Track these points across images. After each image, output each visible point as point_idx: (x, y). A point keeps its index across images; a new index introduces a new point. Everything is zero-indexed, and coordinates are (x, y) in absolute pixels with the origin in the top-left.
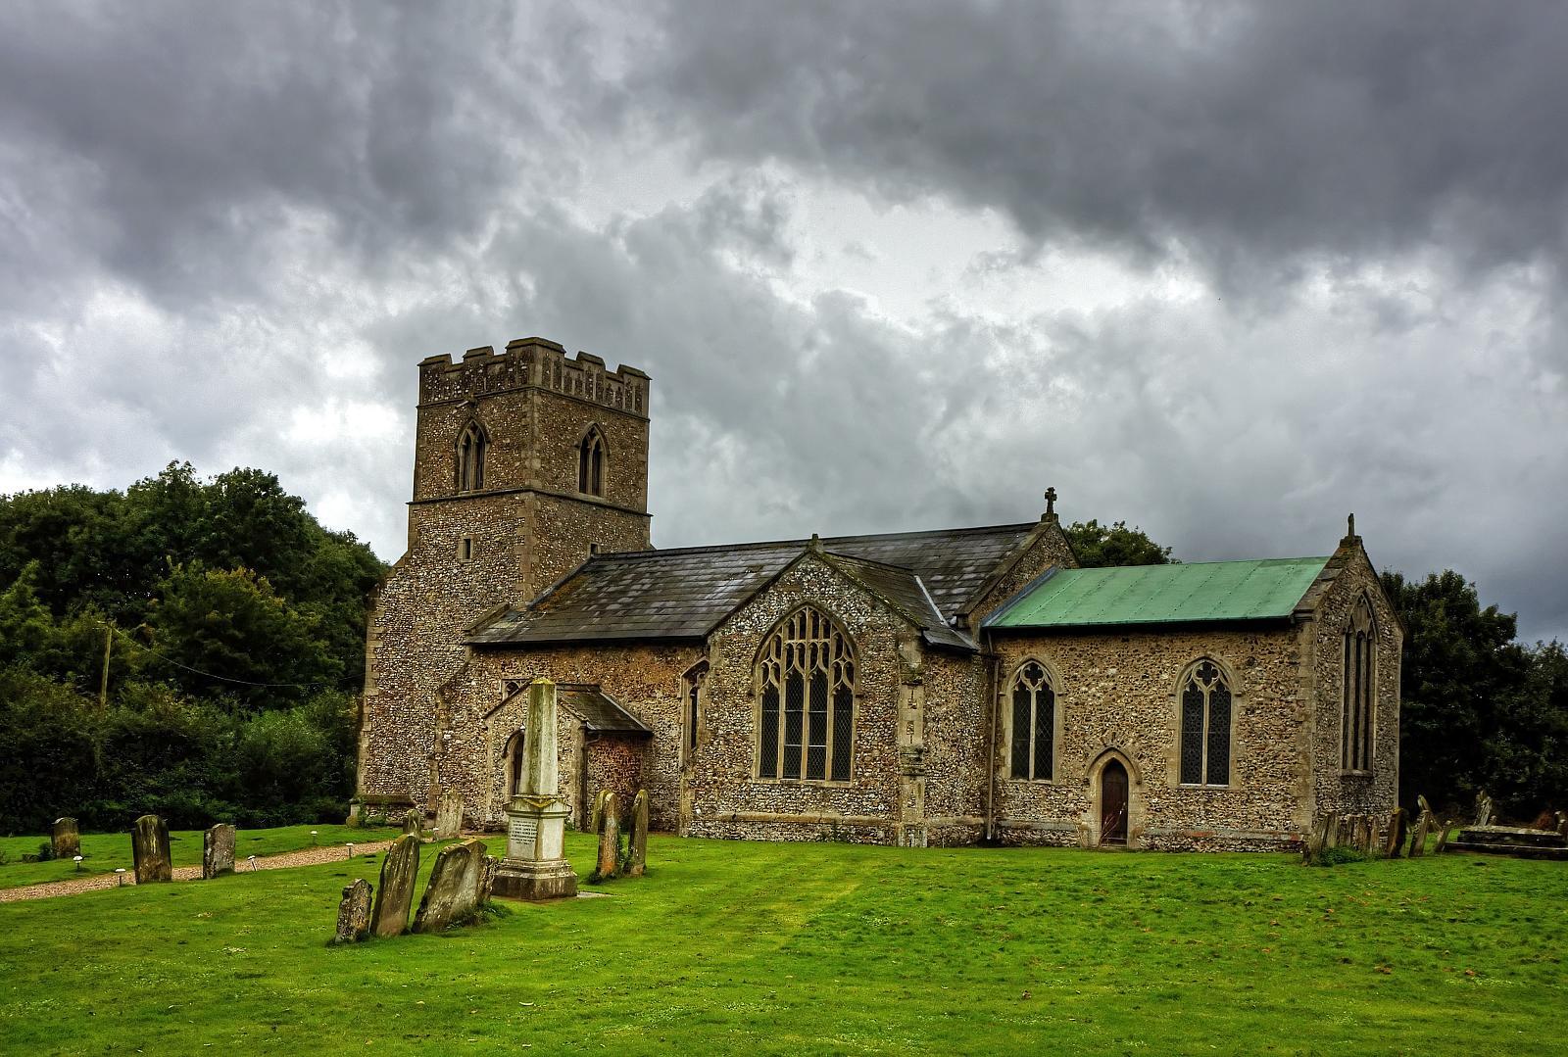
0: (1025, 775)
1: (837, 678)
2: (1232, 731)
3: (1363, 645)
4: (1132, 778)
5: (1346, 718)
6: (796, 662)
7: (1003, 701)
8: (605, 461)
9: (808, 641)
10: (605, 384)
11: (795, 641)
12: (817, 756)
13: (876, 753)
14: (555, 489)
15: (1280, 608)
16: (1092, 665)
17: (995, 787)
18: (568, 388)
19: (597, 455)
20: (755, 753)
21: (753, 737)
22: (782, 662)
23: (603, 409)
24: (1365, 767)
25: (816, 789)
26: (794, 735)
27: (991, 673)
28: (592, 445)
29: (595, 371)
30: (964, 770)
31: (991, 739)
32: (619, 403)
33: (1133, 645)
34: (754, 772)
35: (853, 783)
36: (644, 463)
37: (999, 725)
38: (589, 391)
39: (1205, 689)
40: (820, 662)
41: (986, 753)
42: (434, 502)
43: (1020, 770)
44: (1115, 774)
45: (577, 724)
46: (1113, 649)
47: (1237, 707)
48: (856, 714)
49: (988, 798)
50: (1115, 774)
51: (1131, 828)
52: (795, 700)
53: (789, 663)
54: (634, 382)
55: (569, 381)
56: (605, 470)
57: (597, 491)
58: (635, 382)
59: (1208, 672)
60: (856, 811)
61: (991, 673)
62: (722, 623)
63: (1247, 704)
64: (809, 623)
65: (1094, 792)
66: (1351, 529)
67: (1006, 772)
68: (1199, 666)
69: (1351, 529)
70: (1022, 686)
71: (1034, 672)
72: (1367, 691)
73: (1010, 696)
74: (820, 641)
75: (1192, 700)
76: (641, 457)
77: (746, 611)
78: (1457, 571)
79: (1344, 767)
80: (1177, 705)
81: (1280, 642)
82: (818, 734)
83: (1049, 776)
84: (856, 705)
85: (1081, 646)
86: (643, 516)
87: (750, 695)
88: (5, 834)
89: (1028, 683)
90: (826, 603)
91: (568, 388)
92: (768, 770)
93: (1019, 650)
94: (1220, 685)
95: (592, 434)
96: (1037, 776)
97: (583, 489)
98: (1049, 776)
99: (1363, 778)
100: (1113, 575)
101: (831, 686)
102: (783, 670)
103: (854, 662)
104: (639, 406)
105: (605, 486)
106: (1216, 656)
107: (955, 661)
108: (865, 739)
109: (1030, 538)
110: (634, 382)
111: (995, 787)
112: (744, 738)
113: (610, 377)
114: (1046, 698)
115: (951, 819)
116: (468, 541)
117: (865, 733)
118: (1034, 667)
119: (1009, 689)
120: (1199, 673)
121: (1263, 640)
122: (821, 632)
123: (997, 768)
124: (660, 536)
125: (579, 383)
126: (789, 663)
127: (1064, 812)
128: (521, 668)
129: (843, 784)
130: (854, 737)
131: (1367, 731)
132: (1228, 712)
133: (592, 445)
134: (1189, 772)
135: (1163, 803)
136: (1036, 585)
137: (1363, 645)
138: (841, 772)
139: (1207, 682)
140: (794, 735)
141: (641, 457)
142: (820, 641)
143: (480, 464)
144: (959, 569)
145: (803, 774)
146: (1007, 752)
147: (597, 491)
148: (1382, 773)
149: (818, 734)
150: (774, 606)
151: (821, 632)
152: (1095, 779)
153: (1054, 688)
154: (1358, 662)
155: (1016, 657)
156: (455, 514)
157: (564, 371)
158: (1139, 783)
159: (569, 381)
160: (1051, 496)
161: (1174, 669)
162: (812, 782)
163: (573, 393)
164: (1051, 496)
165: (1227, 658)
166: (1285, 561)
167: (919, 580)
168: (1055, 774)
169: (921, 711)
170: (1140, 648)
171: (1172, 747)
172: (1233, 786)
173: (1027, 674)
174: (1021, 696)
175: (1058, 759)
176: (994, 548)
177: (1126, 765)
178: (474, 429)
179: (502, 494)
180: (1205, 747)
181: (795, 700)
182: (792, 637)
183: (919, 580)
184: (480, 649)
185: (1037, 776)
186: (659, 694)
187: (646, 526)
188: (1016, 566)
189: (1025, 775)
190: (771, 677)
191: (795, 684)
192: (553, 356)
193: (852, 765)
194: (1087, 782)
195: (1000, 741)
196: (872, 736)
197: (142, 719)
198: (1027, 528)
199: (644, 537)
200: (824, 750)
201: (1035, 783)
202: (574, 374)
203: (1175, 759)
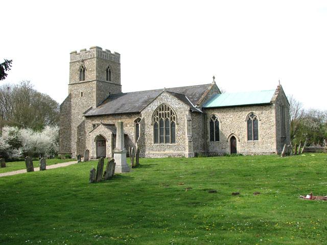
0: (213, 141)
1: (171, 120)
2: (259, 129)
4: (237, 140)
8: (111, 73)
9: (167, 112)
11: (161, 112)
13: (181, 137)
14: (102, 80)
15: (268, 101)
19: (110, 72)
25: (168, 145)
27: (205, 118)
28: (109, 70)
29: (109, 53)
31: (205, 133)
37: (207, 129)
39: (251, 119)
41: (204, 136)
42: (74, 84)
43: (212, 139)
45: (111, 133)
47: (259, 123)
48: (176, 128)
54: (117, 56)
55: (103, 55)
56: (112, 75)
57: (110, 80)
58: (117, 55)
59: (252, 115)
61: (205, 118)
65: (229, 144)
67: (209, 140)
70: (212, 120)
71: (214, 117)
74: (167, 112)
75: (249, 122)
77: (149, 106)
80: (246, 123)
81: (268, 107)
82: (167, 133)
84: (176, 125)
85: (225, 110)
86: (120, 86)
89: (251, 118)
90: (168, 103)
92: (156, 141)
95: (109, 67)
97: (107, 80)
98: (219, 140)
100: (118, 109)
104: (118, 61)
105: (112, 79)
106: (254, 112)
110: (117, 56)
116: (82, 93)
117: (178, 132)
118: (214, 116)
119: (209, 121)
122: (167, 110)
123: (207, 139)
124: (124, 91)
125: (106, 56)
127: (222, 148)
128: (96, 122)
129: (174, 144)
130: (176, 133)
131: (285, 128)
133: (109, 70)
140: (161, 133)
143: (84, 75)
146: (209, 135)
147: (110, 80)
150: (156, 104)
151: (167, 110)
153: (258, 118)
156: (79, 87)
159: (103, 55)
160: (214, 78)
161: (245, 114)
164: (214, 78)
165: (257, 113)
169: (191, 126)
171: (245, 133)
173: (213, 117)
174: (212, 122)
177: (236, 137)
178: (83, 67)
179: (90, 82)
182: (160, 111)
184: (87, 117)
186: (128, 125)
187: (121, 88)
191: (161, 121)
192: (100, 50)
195: (207, 134)
197: (238, 168)
199: (120, 91)
201: (216, 142)
202: (105, 54)
203: (246, 136)
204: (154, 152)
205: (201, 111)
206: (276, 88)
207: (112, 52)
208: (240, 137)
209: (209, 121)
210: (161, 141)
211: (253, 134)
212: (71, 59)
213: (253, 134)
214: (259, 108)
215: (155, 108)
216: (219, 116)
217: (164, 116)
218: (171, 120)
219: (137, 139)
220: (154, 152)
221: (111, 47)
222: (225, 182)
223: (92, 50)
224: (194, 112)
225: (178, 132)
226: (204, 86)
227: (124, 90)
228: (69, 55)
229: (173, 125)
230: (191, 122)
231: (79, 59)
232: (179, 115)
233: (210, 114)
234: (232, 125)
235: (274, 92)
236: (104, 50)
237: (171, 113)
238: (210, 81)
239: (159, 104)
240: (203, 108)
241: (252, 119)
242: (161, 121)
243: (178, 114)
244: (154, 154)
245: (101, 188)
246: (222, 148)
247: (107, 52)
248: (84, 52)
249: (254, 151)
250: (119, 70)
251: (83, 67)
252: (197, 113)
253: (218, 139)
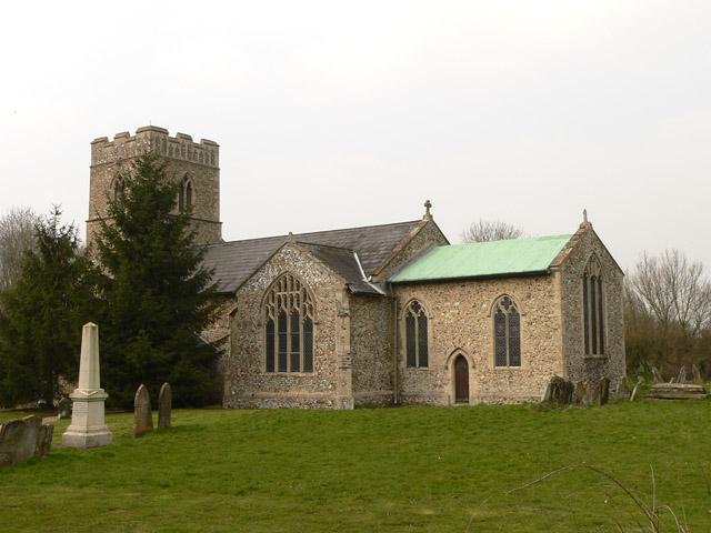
0: (414, 365)
3: (596, 284)
4: (470, 364)
5: (586, 326)
6: (283, 306)
7: (400, 323)
8: (194, 193)
9: (294, 293)
10: (193, 150)
12: (295, 360)
15: (542, 266)
16: (447, 301)
17: (398, 373)
18: (171, 153)
19: (189, 189)
20: (263, 357)
21: (261, 349)
22: (275, 305)
23: (192, 164)
24: (602, 352)
25: (295, 377)
26: (283, 347)
27: (393, 308)
29: (187, 143)
30: (379, 364)
32: (202, 161)
33: (467, 288)
34: (263, 368)
35: (315, 374)
36: (217, 193)
38: (183, 155)
39: (504, 311)
40: (295, 305)
41: (391, 354)
43: (411, 363)
44: (461, 363)
46: (457, 290)
47: (523, 321)
48: (315, 334)
49: (394, 380)
50: (461, 363)
51: (470, 395)
52: (283, 327)
53: (279, 305)
54: (210, 149)
58: (210, 148)
59: (507, 302)
60: (317, 390)
62: (244, 284)
63: (528, 320)
64: (289, 283)
65: (450, 374)
66: (586, 219)
67: (403, 364)
68: (502, 299)
69: (586, 219)
70: (410, 313)
71: (416, 306)
72: (601, 309)
73: (404, 319)
75: (499, 319)
76: (215, 190)
78: (126, 119)
79: (587, 352)
80: (491, 322)
81: (542, 284)
82: (295, 347)
83: (519, 365)
84: (315, 327)
85: (441, 290)
87: (259, 325)
88: (643, 351)
91: (171, 153)
92: (270, 368)
93: (407, 294)
94: (513, 310)
95: (186, 179)
96: (420, 366)
99: (600, 359)
101: (302, 318)
102: (276, 310)
103: (312, 303)
107: (369, 302)
108: (319, 347)
109: (416, 229)
110: (210, 149)
111: (398, 373)
112: (257, 350)
113: (196, 146)
114: (423, 320)
115: (372, 393)
117: (319, 344)
118: (416, 303)
119: (403, 316)
120: (502, 304)
121: (534, 283)
123: (399, 361)
124: (228, 235)
126: (279, 305)
127: (435, 386)
130: (314, 347)
132: (519, 325)
133: (186, 185)
134: (500, 361)
135: (487, 378)
136: (420, 255)
137: (596, 284)
138: (309, 368)
139: (507, 308)
140: (283, 347)
141: (215, 190)
142: (294, 293)
144: (376, 249)
145: (289, 369)
146: (404, 352)
148: (613, 356)
149: (295, 347)
152: (450, 365)
153: (427, 314)
154: (593, 293)
155: (407, 297)
157: (169, 144)
158: (474, 367)
160: (428, 205)
161: (488, 298)
162: (294, 374)
163: (174, 155)
164: (428, 205)
165: (516, 292)
166: (550, 238)
167: (356, 255)
168: (524, 361)
170: (471, 289)
171: (489, 346)
172: (522, 367)
173: (413, 307)
174: (410, 320)
175: (431, 356)
176: (397, 233)
177: (466, 357)
180: (417, 333)
181: (283, 327)
183: (356, 255)
185: (420, 366)
187: (219, 229)
188: (408, 245)
189: (414, 365)
190: (270, 314)
191: (283, 317)
192: (162, 136)
193: (314, 363)
194: (447, 368)
196: (324, 346)
198: (416, 223)
200: (298, 355)
201: (419, 370)
202: (174, 146)
203: (491, 354)
204: (264, 394)
205: (381, 292)
206: (574, 229)
207: (197, 140)
208: (477, 357)
209: (403, 316)
210: (295, 368)
211: (508, 350)
212: (94, 158)
213: (508, 350)
214: (521, 282)
215: (267, 283)
216: (426, 299)
217: (289, 304)
218: (305, 313)
219: (398, 337)
220: (264, 394)
221: (185, 121)
222: (265, 523)
223: (142, 134)
224: (358, 295)
225: (319, 344)
226: (404, 227)
227: (228, 235)
228: (89, 149)
229: (308, 326)
230: (347, 320)
231: (111, 157)
232: (320, 302)
233: (407, 297)
234: (458, 327)
235: (568, 240)
236: (172, 134)
237: (305, 296)
238: (418, 214)
239: (276, 273)
240: (388, 284)
241: (415, 315)
242: (283, 317)
243: (319, 298)
244: (263, 399)
245: (707, 369)
246: (435, 386)
247: (181, 140)
248: (124, 140)
249: (508, 391)
250: (216, 185)
251: (120, 178)
252: (371, 297)
253: (424, 363)
